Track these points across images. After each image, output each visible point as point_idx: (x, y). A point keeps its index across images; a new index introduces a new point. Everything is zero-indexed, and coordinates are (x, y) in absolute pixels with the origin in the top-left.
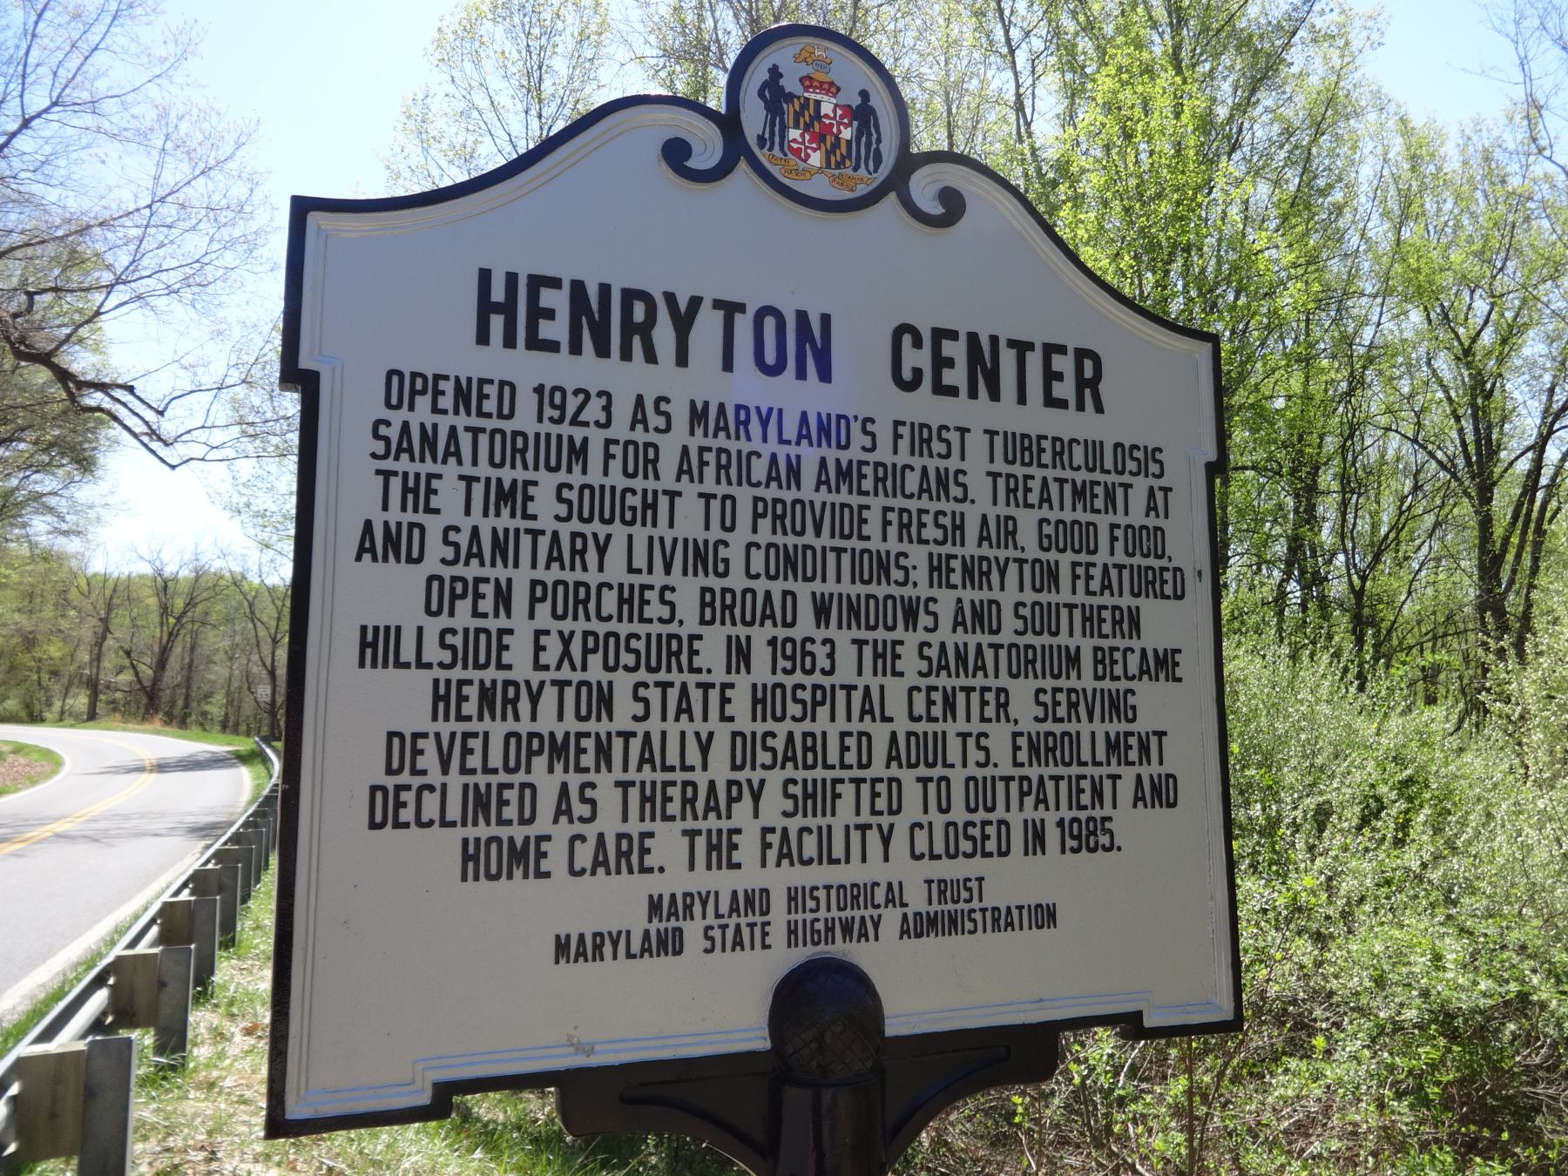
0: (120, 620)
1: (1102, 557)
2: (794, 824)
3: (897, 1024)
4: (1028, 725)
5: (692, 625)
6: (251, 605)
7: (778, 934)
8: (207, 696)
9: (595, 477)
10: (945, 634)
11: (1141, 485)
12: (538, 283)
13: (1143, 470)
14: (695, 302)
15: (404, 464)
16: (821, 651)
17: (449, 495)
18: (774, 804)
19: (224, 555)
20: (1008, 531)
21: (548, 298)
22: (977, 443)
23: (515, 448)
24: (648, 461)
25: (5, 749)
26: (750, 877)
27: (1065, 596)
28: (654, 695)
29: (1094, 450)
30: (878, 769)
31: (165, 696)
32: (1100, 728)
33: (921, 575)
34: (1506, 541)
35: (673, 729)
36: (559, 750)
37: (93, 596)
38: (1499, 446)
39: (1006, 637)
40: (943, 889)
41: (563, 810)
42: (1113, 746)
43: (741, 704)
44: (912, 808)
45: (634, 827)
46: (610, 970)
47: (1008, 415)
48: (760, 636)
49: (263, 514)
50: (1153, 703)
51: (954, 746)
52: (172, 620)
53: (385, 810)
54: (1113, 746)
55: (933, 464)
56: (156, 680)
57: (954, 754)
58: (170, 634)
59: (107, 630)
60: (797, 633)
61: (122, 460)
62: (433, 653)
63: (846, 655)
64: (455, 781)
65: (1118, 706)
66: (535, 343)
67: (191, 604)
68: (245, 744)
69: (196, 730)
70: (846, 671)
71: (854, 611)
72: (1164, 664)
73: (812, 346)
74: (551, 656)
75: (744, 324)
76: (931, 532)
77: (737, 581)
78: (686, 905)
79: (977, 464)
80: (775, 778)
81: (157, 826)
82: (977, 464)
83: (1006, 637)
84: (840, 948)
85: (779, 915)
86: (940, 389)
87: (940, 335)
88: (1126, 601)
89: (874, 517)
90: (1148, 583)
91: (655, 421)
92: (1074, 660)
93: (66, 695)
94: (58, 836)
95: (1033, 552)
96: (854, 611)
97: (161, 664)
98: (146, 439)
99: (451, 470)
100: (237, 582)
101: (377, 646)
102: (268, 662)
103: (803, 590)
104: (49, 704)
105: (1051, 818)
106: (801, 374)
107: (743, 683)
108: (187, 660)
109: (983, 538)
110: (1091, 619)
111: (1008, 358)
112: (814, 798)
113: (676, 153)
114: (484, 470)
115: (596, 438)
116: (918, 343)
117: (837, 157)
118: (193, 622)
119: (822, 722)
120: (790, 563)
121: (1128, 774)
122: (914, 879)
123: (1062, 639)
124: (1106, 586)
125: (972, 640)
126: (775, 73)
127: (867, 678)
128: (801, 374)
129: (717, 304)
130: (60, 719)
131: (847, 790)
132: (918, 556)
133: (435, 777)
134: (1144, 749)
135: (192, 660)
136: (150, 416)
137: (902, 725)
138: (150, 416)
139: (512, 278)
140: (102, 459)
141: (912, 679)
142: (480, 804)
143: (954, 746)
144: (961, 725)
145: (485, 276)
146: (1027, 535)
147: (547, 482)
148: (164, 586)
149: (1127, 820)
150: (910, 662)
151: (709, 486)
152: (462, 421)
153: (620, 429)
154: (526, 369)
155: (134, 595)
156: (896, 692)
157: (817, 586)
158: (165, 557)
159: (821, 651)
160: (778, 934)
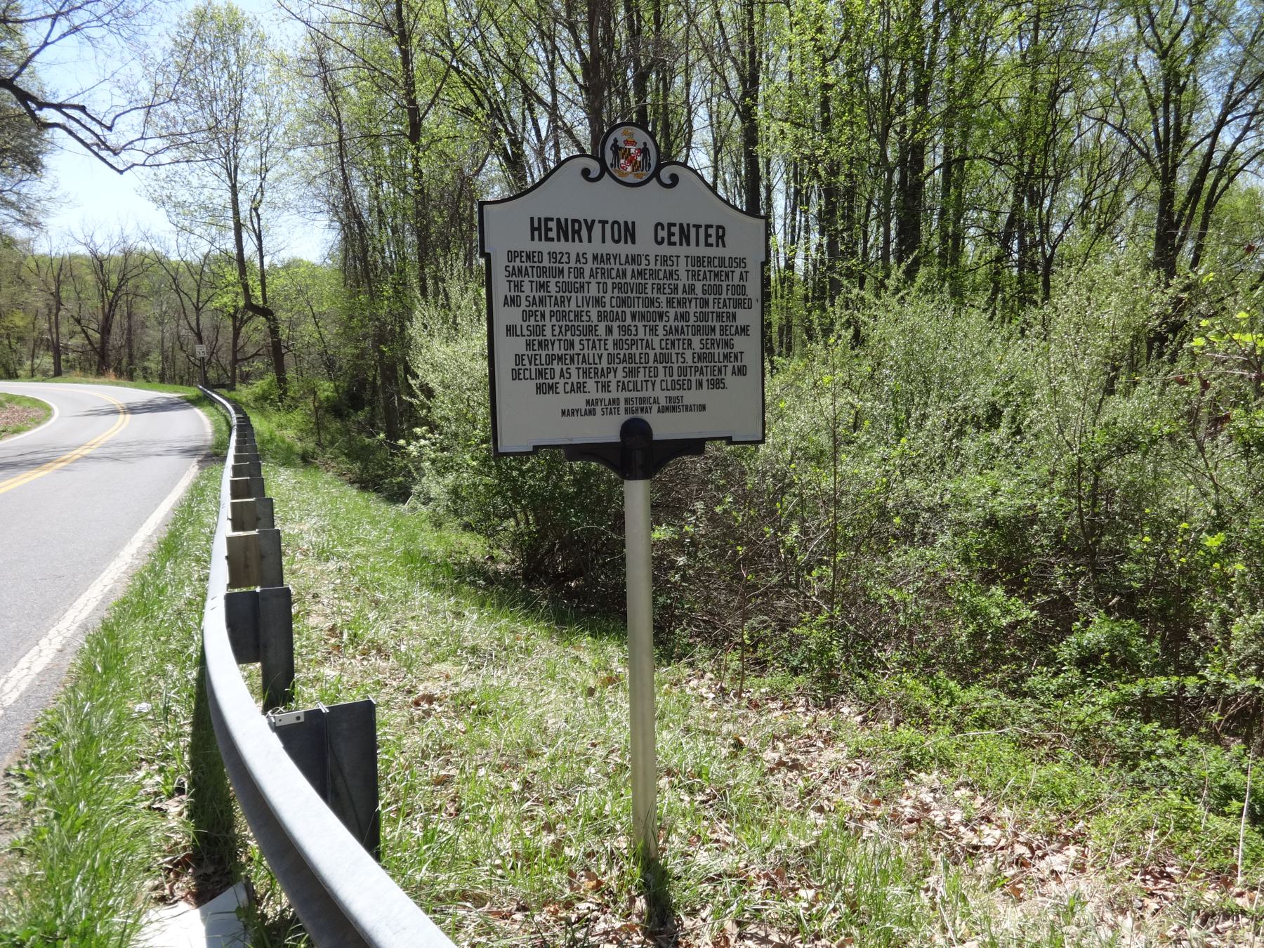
1: (724, 296)
5: (595, 322)
7: (622, 411)
8: (145, 355)
9: (566, 279)
10: (672, 322)
11: (738, 271)
13: (738, 266)
14: (593, 221)
15: (514, 278)
16: (633, 329)
17: (526, 286)
18: (620, 374)
22: (682, 260)
23: (544, 271)
24: (580, 272)
25: (3, 399)
27: (711, 309)
29: (722, 260)
30: (651, 364)
31: (112, 355)
33: (664, 304)
34: (1181, 214)
35: (591, 353)
36: (560, 359)
37: (42, 274)
39: (691, 323)
40: (671, 399)
41: (562, 375)
42: (725, 356)
43: (610, 345)
45: (581, 380)
46: (576, 419)
47: (693, 251)
48: (615, 325)
49: (182, 205)
50: (739, 343)
51: (674, 357)
52: (110, 294)
53: (516, 375)
54: (725, 356)
55: (668, 268)
56: (104, 341)
58: (111, 305)
59: (59, 303)
60: (626, 324)
61: (65, 160)
62: (525, 332)
63: (641, 330)
64: (533, 367)
65: (727, 344)
66: (548, 239)
67: (123, 279)
68: (192, 392)
69: (141, 381)
70: (641, 335)
71: (643, 317)
72: (744, 330)
73: (629, 232)
74: (556, 332)
75: (608, 227)
76: (667, 291)
77: (608, 308)
78: (597, 402)
79: (682, 267)
80: (620, 367)
81: (154, 449)
82: (682, 267)
83: (691, 323)
84: (640, 415)
85: (622, 405)
86: (671, 244)
87: (671, 225)
88: (732, 310)
89: (649, 287)
90: (740, 304)
91: (583, 260)
92: (713, 330)
93: (33, 356)
95: (700, 295)
96: (643, 317)
97: (105, 330)
98: (95, 148)
99: (526, 279)
100: (160, 260)
101: (511, 330)
102: (194, 324)
103: (628, 311)
104: (20, 363)
105: (705, 378)
107: (610, 339)
111: (693, 231)
112: (632, 372)
113: (586, 173)
114: (535, 279)
115: (566, 267)
116: (663, 229)
117: (637, 167)
118: (127, 294)
119: (634, 350)
120: (624, 302)
121: (730, 366)
122: (662, 396)
123: (710, 323)
124: (725, 305)
125: (680, 324)
126: (616, 141)
128: (626, 242)
129: (600, 222)
130: (32, 375)
131: (642, 370)
132: (663, 298)
133: (528, 366)
134: (736, 357)
135: (130, 326)
137: (658, 351)
140: (46, 159)
141: (661, 337)
142: (540, 374)
143: (674, 357)
145: (532, 219)
146: (699, 290)
147: (553, 281)
148: (99, 264)
149: (729, 379)
150: (661, 332)
151: (599, 280)
152: (529, 264)
153: (572, 264)
154: (545, 247)
155: (75, 273)
156: (656, 340)
157: (632, 309)
158: (98, 240)
159: (633, 329)
160: (622, 411)
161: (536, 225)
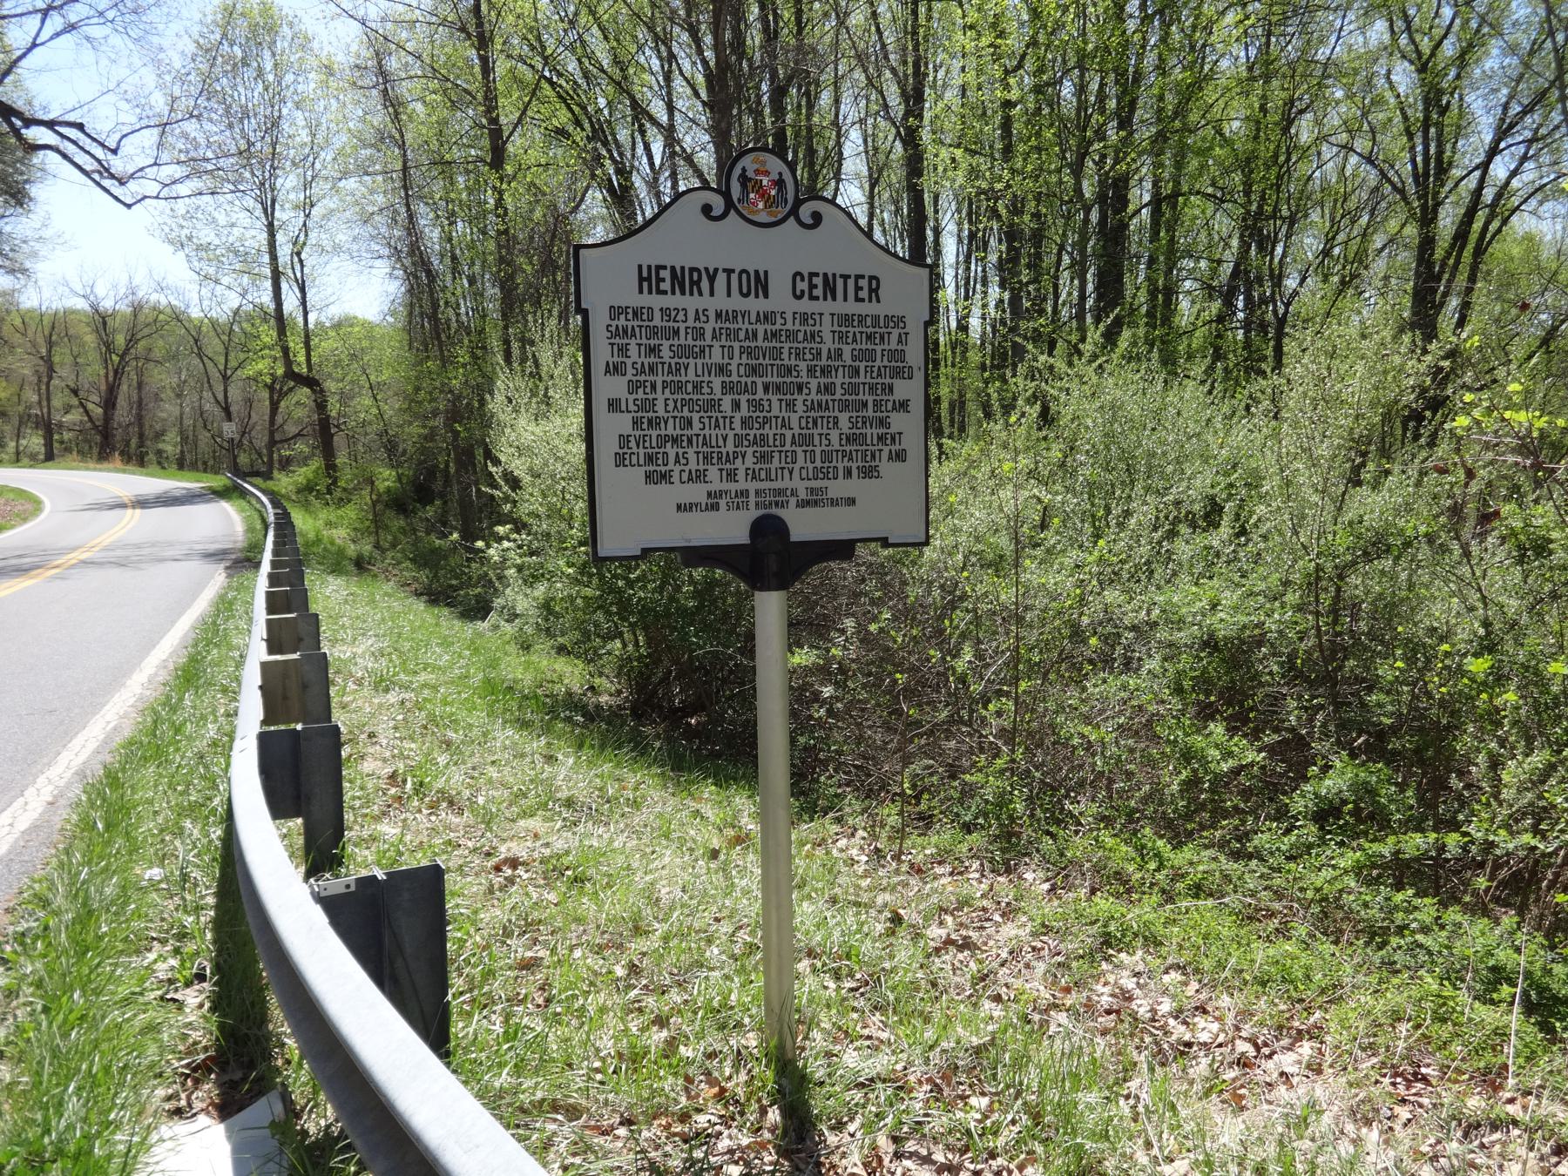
0: (61, 356)
2: (757, 467)
3: (793, 538)
4: (846, 430)
5: (719, 396)
6: (196, 341)
7: (752, 505)
8: (159, 435)
9: (682, 341)
10: (813, 396)
11: (895, 332)
12: (659, 268)
13: (896, 326)
14: (716, 270)
15: (617, 340)
16: (766, 404)
17: (633, 351)
18: (750, 460)
19: (161, 289)
20: (839, 354)
21: (663, 274)
22: (827, 319)
23: (654, 332)
24: (700, 334)
26: (742, 484)
27: (862, 379)
28: (706, 421)
29: (876, 318)
31: (119, 434)
32: (875, 431)
33: (804, 373)
34: (1444, 264)
35: (714, 433)
37: (30, 333)
38: (1450, 164)
41: (677, 461)
43: (737, 424)
44: (801, 461)
45: (701, 467)
47: (840, 307)
48: (744, 398)
50: (898, 421)
51: (817, 438)
53: (620, 460)
55: (808, 329)
56: (108, 418)
57: (817, 442)
58: (116, 372)
59: (51, 369)
60: (757, 397)
62: (632, 407)
63: (775, 405)
64: (642, 451)
65: (882, 422)
66: (660, 292)
67: (132, 340)
68: (218, 481)
69: (155, 468)
72: (903, 406)
73: (759, 284)
74: (670, 408)
75: (734, 277)
76: (808, 356)
77: (734, 378)
79: (826, 328)
80: (750, 450)
81: (170, 553)
82: (826, 328)
86: (812, 298)
87: (812, 275)
88: (888, 380)
90: (898, 373)
91: (703, 318)
92: (865, 405)
94: (84, 562)
95: (849, 362)
96: (778, 388)
97: (109, 403)
98: (96, 176)
99: (633, 342)
100: (178, 317)
101: (614, 405)
102: (221, 397)
103: (759, 381)
106: (757, 296)
107: (738, 416)
108: (135, 398)
109: (829, 357)
110: (873, 389)
111: (840, 282)
112: (764, 458)
113: (707, 210)
114: (644, 341)
115: (682, 326)
117: (770, 203)
119: (767, 430)
120: (754, 371)
121: (886, 449)
123: (861, 397)
124: (879, 375)
126: (744, 170)
127: (784, 413)
128: (757, 296)
131: (776, 455)
132: (803, 366)
133: (635, 450)
134: (893, 439)
136: (99, 152)
137: (797, 431)
138: (99, 152)
139: (649, 267)
140: (33, 190)
141: (800, 413)
142: (650, 459)
143: (817, 438)
144: (820, 431)
145: (640, 267)
146: (847, 356)
147: (666, 344)
148: (101, 321)
149: (885, 466)
150: (800, 407)
151: (723, 342)
152: (636, 323)
153: (690, 323)
154: (657, 302)
156: (794, 418)
157: (764, 379)
158: (100, 291)
159: (766, 404)
160: (752, 505)
161: (645, 274)
